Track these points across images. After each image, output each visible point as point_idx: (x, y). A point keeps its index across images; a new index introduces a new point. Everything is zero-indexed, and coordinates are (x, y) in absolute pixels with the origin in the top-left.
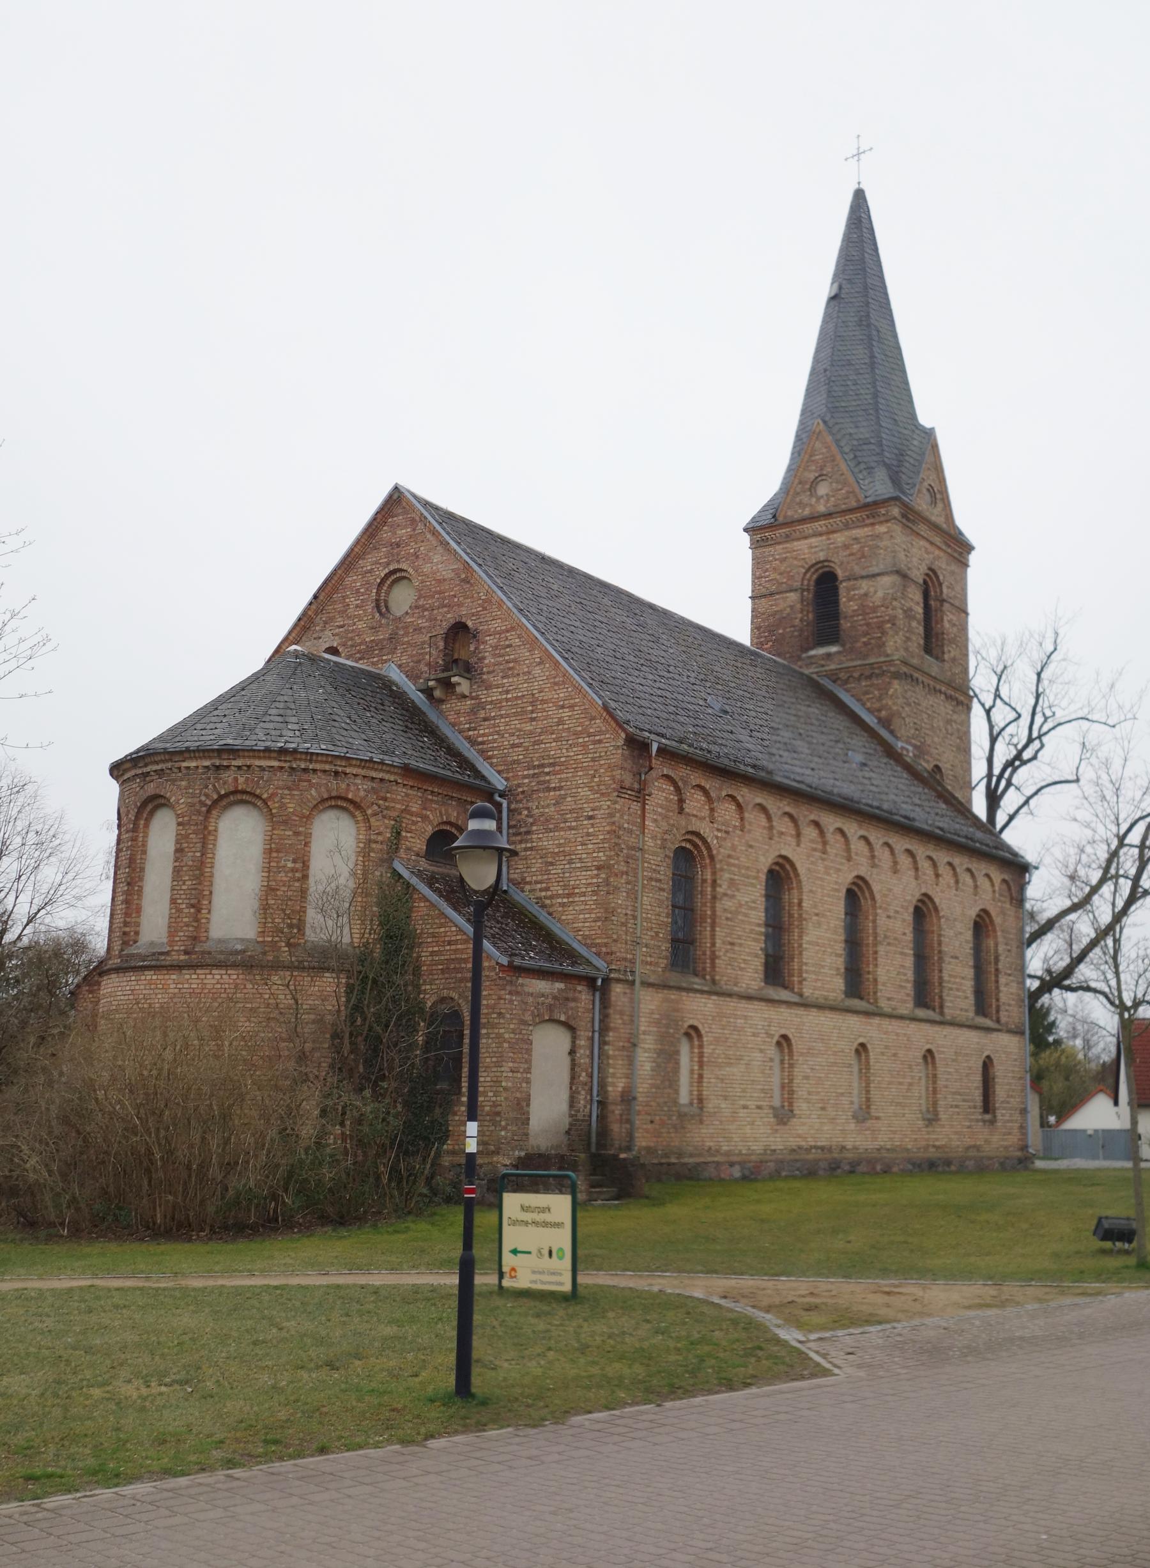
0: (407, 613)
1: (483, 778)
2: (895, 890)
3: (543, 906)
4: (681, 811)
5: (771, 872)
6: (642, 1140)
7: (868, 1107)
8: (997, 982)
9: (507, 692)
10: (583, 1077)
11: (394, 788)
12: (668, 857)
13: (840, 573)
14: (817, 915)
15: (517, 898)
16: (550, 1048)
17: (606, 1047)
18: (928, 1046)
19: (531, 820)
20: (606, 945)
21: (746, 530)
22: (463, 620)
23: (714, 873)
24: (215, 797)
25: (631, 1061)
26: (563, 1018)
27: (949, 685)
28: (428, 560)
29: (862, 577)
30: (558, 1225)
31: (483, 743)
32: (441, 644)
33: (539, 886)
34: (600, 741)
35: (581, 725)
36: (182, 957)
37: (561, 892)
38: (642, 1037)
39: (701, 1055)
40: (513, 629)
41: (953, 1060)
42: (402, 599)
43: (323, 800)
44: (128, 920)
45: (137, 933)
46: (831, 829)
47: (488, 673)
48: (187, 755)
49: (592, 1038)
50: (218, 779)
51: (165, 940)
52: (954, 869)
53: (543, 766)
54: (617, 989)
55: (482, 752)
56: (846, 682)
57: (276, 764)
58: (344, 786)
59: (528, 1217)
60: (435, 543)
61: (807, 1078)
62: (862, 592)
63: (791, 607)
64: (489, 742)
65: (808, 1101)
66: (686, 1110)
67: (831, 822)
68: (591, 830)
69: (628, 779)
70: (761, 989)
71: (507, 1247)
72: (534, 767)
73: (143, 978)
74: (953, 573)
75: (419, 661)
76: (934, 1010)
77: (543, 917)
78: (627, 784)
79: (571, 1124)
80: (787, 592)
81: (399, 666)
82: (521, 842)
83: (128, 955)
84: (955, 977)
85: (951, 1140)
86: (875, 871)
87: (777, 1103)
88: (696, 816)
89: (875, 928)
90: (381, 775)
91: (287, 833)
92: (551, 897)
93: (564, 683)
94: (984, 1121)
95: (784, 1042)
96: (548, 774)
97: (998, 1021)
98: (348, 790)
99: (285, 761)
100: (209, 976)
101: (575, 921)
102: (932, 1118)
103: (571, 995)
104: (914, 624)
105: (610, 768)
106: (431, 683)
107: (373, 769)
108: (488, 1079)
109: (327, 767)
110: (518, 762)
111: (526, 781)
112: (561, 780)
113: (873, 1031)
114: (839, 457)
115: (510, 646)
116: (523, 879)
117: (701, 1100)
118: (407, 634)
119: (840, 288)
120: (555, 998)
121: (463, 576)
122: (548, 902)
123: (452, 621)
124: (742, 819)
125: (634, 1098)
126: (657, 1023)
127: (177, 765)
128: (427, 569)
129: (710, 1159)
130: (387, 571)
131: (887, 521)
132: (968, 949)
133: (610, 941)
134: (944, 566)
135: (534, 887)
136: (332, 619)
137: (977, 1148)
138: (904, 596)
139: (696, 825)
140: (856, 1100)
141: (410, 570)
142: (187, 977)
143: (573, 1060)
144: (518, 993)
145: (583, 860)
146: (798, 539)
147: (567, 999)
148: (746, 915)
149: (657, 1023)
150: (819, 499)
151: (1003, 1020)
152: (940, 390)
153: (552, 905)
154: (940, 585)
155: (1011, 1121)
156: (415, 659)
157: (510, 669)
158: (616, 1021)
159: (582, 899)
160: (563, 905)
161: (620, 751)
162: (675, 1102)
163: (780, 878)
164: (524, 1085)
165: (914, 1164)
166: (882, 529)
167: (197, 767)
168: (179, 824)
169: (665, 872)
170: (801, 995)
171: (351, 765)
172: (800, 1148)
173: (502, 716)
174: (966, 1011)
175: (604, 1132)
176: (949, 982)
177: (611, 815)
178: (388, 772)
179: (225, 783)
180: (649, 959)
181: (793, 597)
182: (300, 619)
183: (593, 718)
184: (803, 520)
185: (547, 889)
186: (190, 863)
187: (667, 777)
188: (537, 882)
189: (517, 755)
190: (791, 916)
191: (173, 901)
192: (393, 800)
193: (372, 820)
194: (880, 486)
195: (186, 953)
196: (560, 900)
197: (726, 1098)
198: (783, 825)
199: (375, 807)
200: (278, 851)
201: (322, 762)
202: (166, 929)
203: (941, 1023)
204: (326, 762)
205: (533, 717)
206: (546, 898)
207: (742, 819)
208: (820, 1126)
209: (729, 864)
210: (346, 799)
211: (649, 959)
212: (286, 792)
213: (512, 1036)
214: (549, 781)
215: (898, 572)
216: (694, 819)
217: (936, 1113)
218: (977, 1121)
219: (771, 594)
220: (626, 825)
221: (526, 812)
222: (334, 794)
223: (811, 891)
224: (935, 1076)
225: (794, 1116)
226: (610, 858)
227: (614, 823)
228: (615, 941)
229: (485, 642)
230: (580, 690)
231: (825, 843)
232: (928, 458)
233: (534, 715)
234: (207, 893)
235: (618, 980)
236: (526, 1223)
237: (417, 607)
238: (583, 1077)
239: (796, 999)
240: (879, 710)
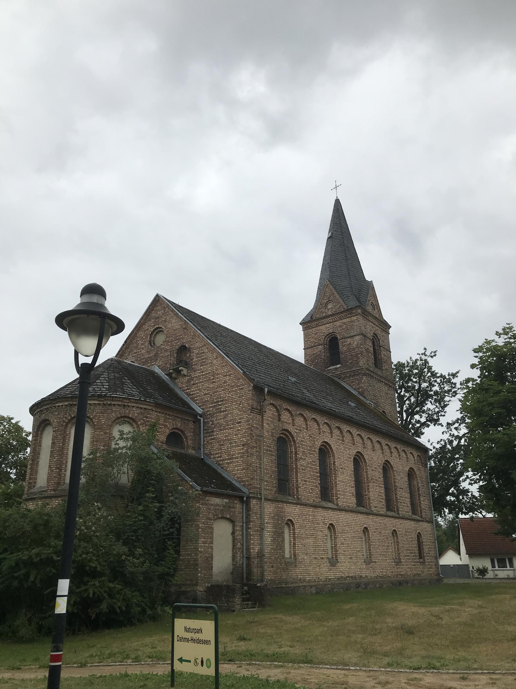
1: (193, 409)
2: (375, 458)
3: (219, 465)
4: (279, 420)
5: (320, 449)
6: (269, 576)
7: (370, 557)
8: (420, 499)
9: (203, 372)
10: (239, 545)
11: (151, 412)
12: (275, 440)
14: (342, 468)
15: (207, 462)
16: (222, 531)
17: (249, 530)
18: (394, 528)
20: (247, 481)
21: (300, 324)
23: (295, 449)
24: (70, 418)
25: (261, 537)
26: (228, 516)
27: (385, 379)
28: (170, 322)
29: (348, 337)
30: (207, 642)
31: (193, 394)
33: (217, 455)
34: (242, 389)
35: (234, 382)
36: (52, 493)
37: (227, 458)
38: (266, 525)
39: (294, 534)
40: (205, 345)
41: (405, 535)
42: (160, 339)
43: (118, 418)
44: (31, 477)
45: (35, 483)
46: (345, 431)
48: (58, 400)
49: (243, 526)
50: (71, 410)
51: (46, 485)
52: (398, 450)
53: (218, 402)
54: (254, 502)
55: (192, 399)
56: (344, 378)
57: (97, 402)
58: (127, 412)
59: (189, 635)
61: (342, 544)
62: (348, 343)
63: (320, 351)
64: (195, 394)
66: (287, 560)
67: (345, 428)
68: (239, 428)
69: (255, 405)
70: (319, 502)
71: (176, 657)
72: (215, 403)
74: (383, 336)
75: (166, 363)
77: (219, 470)
78: (255, 407)
79: (233, 569)
81: (158, 366)
82: (209, 436)
83: (30, 493)
84: (402, 497)
85: (407, 571)
86: (365, 450)
87: (330, 556)
89: (367, 475)
90: (145, 407)
91: (101, 433)
92: (223, 460)
94: (420, 562)
95: (331, 527)
96: (220, 405)
97: (421, 517)
98: (129, 413)
99: (101, 401)
101: (234, 471)
102: (398, 562)
103: (232, 505)
104: (370, 355)
105: (247, 400)
106: (171, 371)
107: (141, 404)
108: (192, 547)
109: (120, 403)
110: (208, 401)
112: (226, 407)
113: (370, 522)
114: (336, 293)
115: (203, 353)
116: (210, 453)
117: (295, 555)
119: (332, 233)
120: (224, 507)
122: (221, 462)
123: (180, 345)
124: (307, 424)
125: (264, 555)
126: (273, 518)
127: (54, 405)
128: (169, 326)
129: (301, 585)
131: (356, 315)
132: (406, 485)
133: (249, 479)
134: (379, 332)
136: (132, 350)
137: (419, 575)
138: (365, 343)
139: (286, 426)
140: (365, 554)
141: (163, 327)
143: (233, 537)
144: (206, 504)
145: (235, 442)
146: (321, 325)
147: (230, 507)
149: (273, 518)
151: (424, 516)
152: (373, 262)
153: (223, 464)
154: (379, 340)
155: (431, 562)
157: (204, 362)
158: (253, 517)
159: (236, 460)
160: (228, 463)
161: (251, 392)
162: (283, 556)
163: (325, 451)
164: (210, 550)
165: (392, 584)
166: (355, 318)
167: (62, 406)
168: (54, 431)
169: (273, 448)
170: (338, 505)
171: (131, 402)
172: (342, 577)
173: (200, 382)
174: (408, 512)
175: (249, 573)
176: (400, 499)
177: (248, 421)
178: (148, 405)
179: (74, 412)
180: (268, 488)
182: (119, 352)
183: (239, 379)
184: (324, 318)
185: (221, 457)
186: (58, 449)
187: (272, 404)
188: (216, 454)
189: (207, 398)
190: (331, 469)
191: (50, 467)
192: (151, 418)
193: (141, 426)
194: (353, 303)
195: (54, 490)
196: (226, 461)
198: (325, 428)
199: (142, 421)
200: (97, 442)
201: (117, 401)
202: (46, 481)
204: (119, 401)
205: (213, 384)
206: (220, 460)
207: (307, 424)
208: (350, 567)
210: (129, 417)
211: (268, 488)
213: (203, 525)
215: (362, 334)
217: (400, 559)
218: (417, 562)
219: (312, 347)
220: (255, 425)
222: (123, 415)
223: (339, 458)
224: (398, 542)
225: (338, 562)
226: (248, 440)
227: (249, 424)
228: (251, 479)
229: (193, 352)
230: (232, 367)
231: (343, 437)
232: (371, 292)
234: (65, 462)
235: (254, 498)
236: (187, 640)
237: (166, 342)
238: (239, 545)
239: (336, 507)
240: (359, 389)
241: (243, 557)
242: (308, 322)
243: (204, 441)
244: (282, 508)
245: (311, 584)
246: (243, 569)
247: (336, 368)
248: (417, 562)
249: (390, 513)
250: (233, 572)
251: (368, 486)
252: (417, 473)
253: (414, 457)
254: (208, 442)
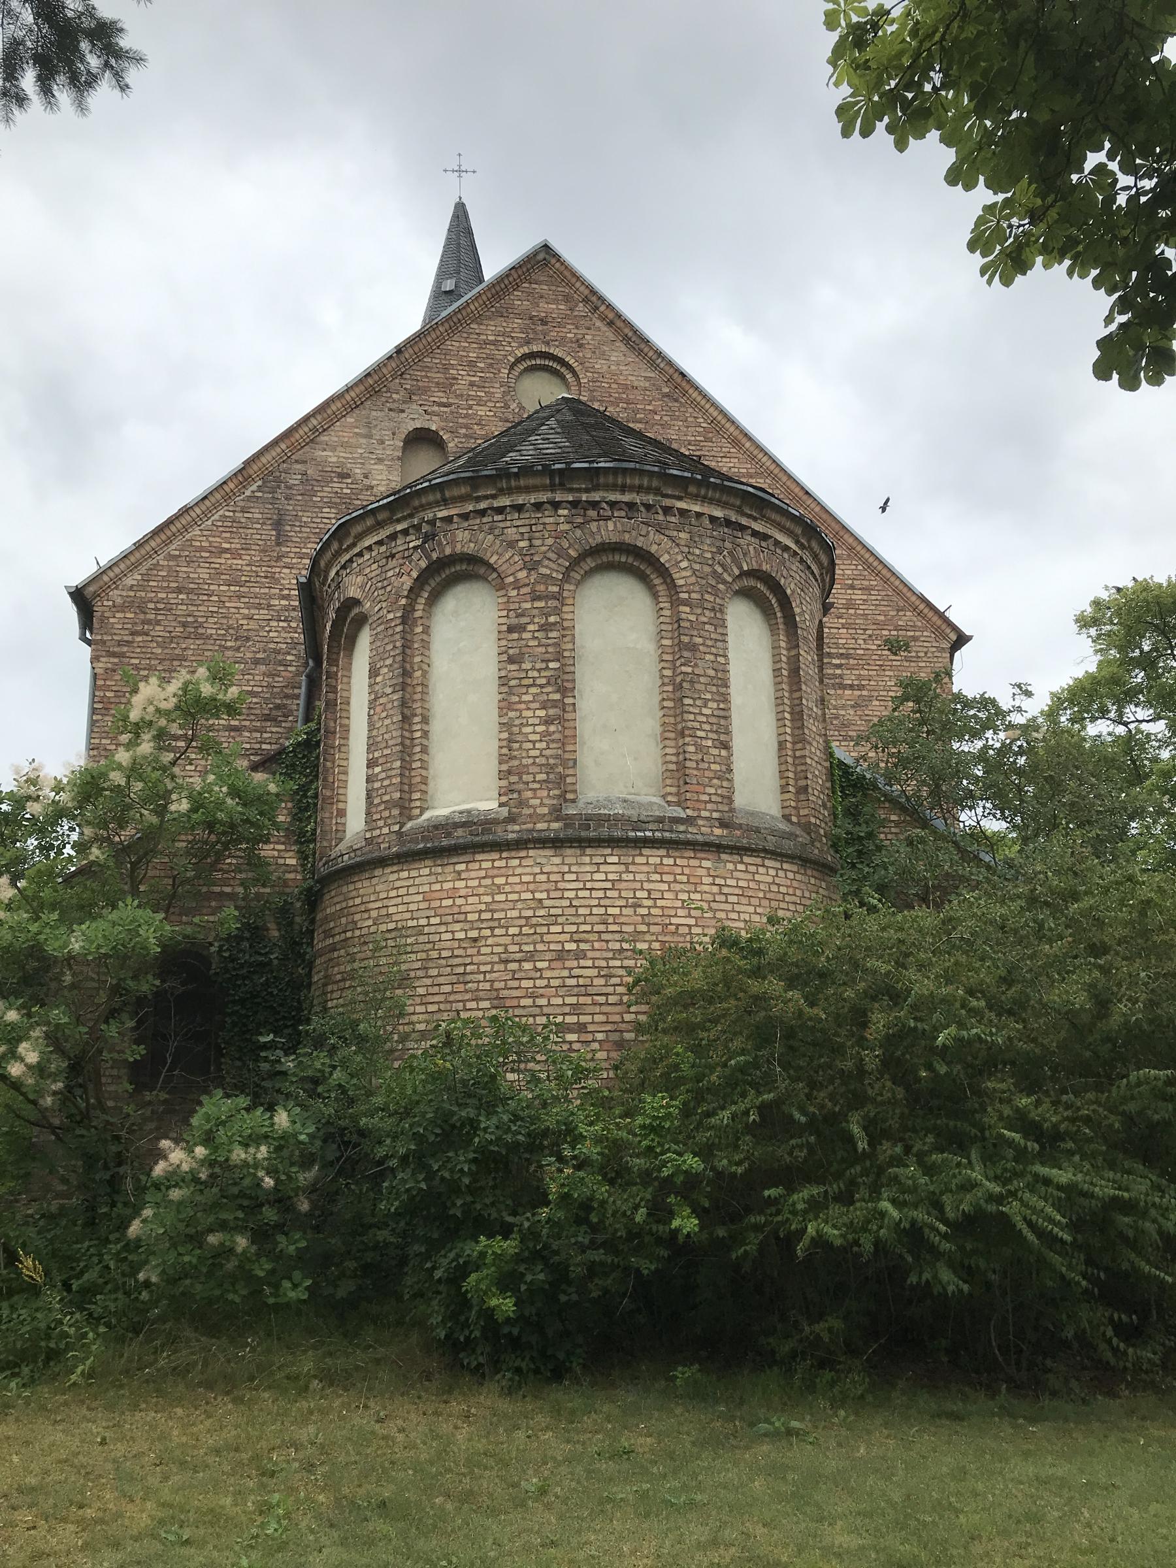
73: (639, 860)
96: (839, 666)
100: (762, 870)
127: (667, 502)
128: (600, 365)
130: (526, 350)
142: (730, 866)
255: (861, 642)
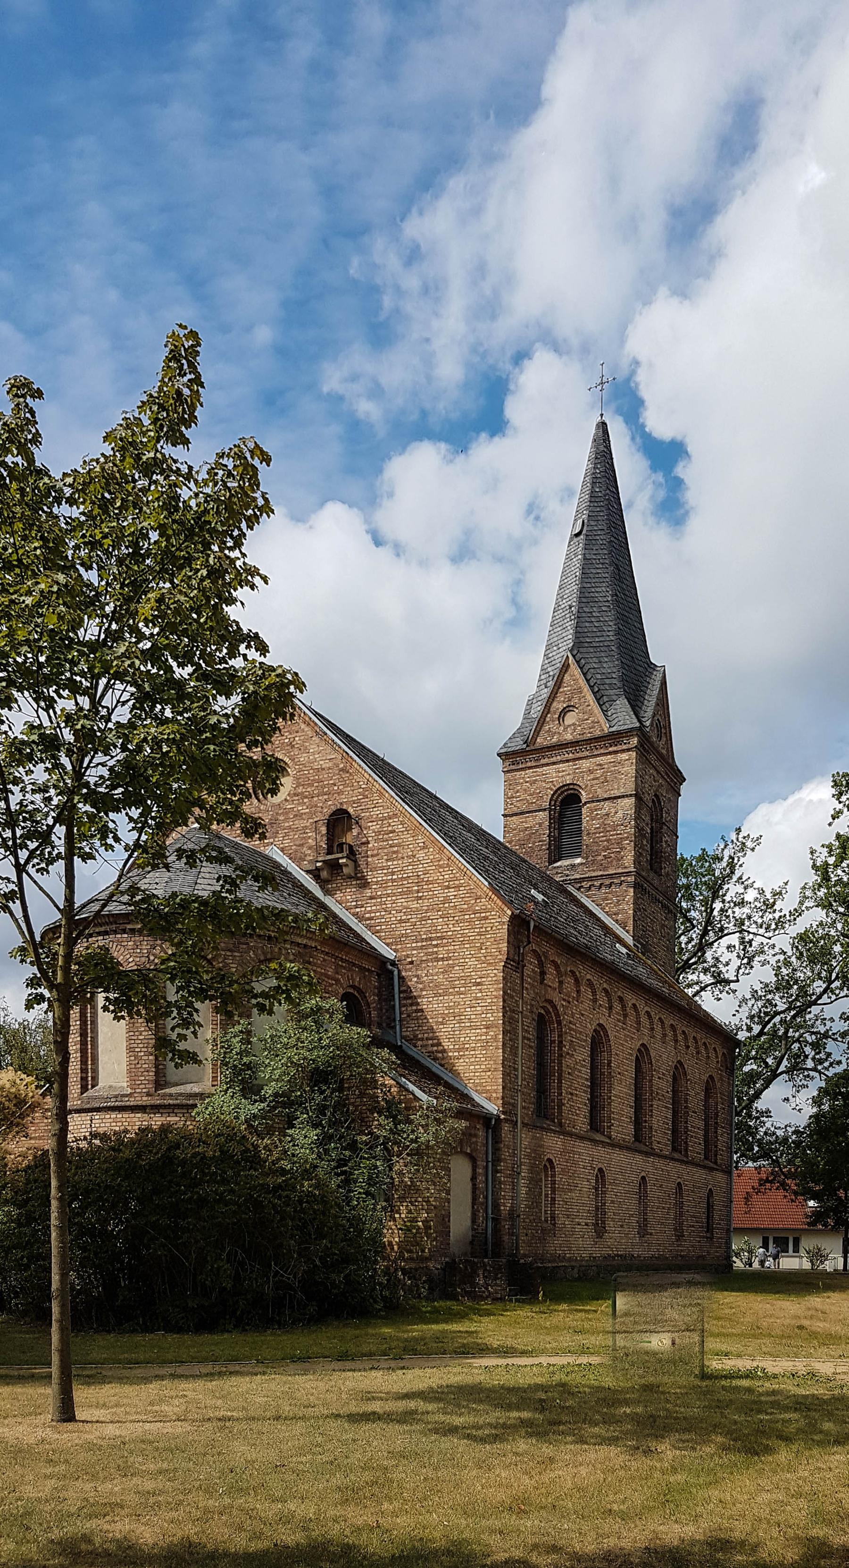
0: (286, 800)
2: (664, 1056)
3: (435, 1059)
4: (542, 982)
7: (646, 1225)
8: (716, 1132)
9: (393, 873)
13: (584, 796)
14: (619, 1074)
17: (498, 1175)
19: (421, 986)
21: (499, 755)
22: (345, 807)
23: (560, 1036)
25: (514, 1186)
29: (605, 799)
31: (371, 919)
32: (324, 830)
33: (430, 1042)
34: (486, 918)
39: (554, 1182)
40: (395, 815)
47: (372, 856)
49: (487, 1167)
53: (431, 939)
55: (369, 927)
58: (276, 950)
60: (310, 733)
61: (613, 1202)
62: (604, 812)
63: (540, 824)
65: (613, 1220)
68: (480, 995)
72: (422, 940)
75: (302, 845)
76: (681, 1152)
80: (536, 811)
81: (282, 850)
88: (550, 987)
89: (651, 1086)
93: (448, 866)
94: (707, 1238)
96: (436, 946)
97: (716, 1163)
103: (473, 1132)
104: (645, 843)
111: (415, 952)
114: (586, 689)
115: (393, 832)
116: (416, 1036)
118: (286, 820)
121: (341, 766)
122: (440, 1055)
123: (333, 808)
127: (122, 927)
135: (425, 1043)
137: (703, 1257)
141: (286, 760)
147: (471, 1135)
148: (580, 1071)
150: (566, 729)
151: (719, 1161)
155: (721, 1238)
156: (297, 843)
157: (394, 852)
158: (505, 1154)
170: (610, 1137)
172: (609, 1255)
173: (388, 895)
181: (543, 816)
188: (427, 1039)
191: (130, 1050)
197: (568, 1216)
203: (686, 1163)
207: (578, 992)
209: (571, 1029)
212: (228, 953)
214: (436, 953)
216: (549, 989)
221: (415, 979)
223: (616, 1054)
233: (421, 894)
237: (296, 795)
241: (487, 1217)
242: (514, 753)
243: (401, 1013)
244: (541, 1139)
245: (573, 1264)
246: (486, 1237)
247: (573, 866)
248: (704, 1237)
249: (676, 1155)
250: (473, 1240)
251: (652, 1106)
252: (718, 1085)
253: (717, 1057)
254: (409, 1016)
255: (451, 926)
